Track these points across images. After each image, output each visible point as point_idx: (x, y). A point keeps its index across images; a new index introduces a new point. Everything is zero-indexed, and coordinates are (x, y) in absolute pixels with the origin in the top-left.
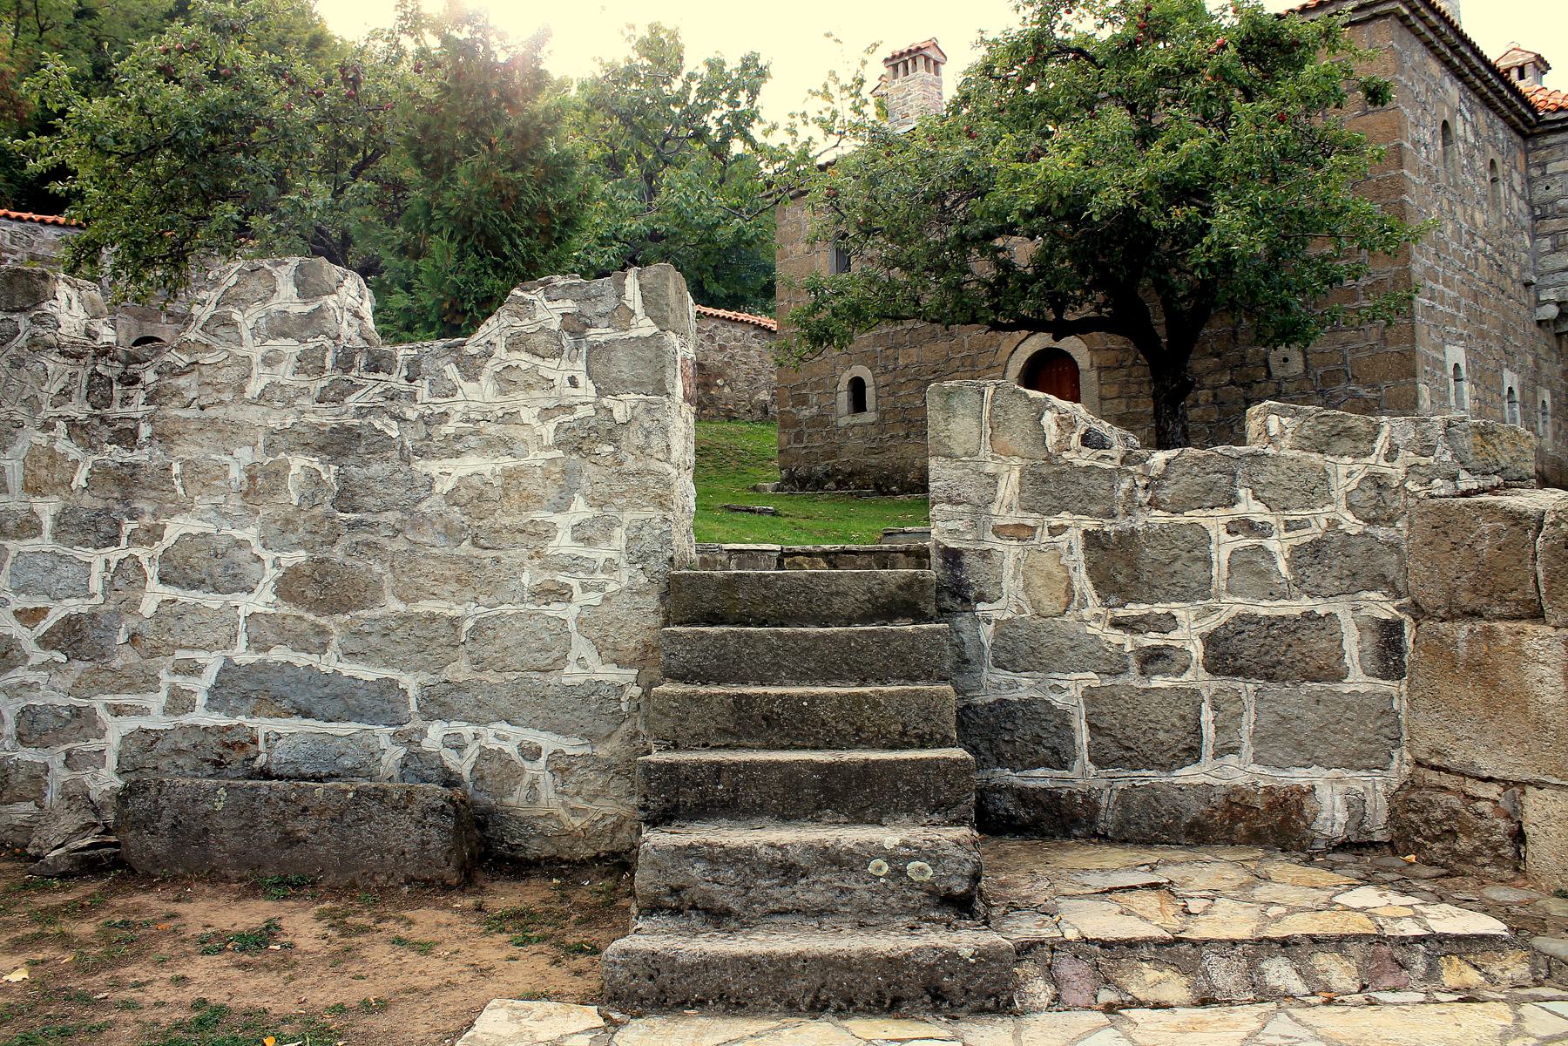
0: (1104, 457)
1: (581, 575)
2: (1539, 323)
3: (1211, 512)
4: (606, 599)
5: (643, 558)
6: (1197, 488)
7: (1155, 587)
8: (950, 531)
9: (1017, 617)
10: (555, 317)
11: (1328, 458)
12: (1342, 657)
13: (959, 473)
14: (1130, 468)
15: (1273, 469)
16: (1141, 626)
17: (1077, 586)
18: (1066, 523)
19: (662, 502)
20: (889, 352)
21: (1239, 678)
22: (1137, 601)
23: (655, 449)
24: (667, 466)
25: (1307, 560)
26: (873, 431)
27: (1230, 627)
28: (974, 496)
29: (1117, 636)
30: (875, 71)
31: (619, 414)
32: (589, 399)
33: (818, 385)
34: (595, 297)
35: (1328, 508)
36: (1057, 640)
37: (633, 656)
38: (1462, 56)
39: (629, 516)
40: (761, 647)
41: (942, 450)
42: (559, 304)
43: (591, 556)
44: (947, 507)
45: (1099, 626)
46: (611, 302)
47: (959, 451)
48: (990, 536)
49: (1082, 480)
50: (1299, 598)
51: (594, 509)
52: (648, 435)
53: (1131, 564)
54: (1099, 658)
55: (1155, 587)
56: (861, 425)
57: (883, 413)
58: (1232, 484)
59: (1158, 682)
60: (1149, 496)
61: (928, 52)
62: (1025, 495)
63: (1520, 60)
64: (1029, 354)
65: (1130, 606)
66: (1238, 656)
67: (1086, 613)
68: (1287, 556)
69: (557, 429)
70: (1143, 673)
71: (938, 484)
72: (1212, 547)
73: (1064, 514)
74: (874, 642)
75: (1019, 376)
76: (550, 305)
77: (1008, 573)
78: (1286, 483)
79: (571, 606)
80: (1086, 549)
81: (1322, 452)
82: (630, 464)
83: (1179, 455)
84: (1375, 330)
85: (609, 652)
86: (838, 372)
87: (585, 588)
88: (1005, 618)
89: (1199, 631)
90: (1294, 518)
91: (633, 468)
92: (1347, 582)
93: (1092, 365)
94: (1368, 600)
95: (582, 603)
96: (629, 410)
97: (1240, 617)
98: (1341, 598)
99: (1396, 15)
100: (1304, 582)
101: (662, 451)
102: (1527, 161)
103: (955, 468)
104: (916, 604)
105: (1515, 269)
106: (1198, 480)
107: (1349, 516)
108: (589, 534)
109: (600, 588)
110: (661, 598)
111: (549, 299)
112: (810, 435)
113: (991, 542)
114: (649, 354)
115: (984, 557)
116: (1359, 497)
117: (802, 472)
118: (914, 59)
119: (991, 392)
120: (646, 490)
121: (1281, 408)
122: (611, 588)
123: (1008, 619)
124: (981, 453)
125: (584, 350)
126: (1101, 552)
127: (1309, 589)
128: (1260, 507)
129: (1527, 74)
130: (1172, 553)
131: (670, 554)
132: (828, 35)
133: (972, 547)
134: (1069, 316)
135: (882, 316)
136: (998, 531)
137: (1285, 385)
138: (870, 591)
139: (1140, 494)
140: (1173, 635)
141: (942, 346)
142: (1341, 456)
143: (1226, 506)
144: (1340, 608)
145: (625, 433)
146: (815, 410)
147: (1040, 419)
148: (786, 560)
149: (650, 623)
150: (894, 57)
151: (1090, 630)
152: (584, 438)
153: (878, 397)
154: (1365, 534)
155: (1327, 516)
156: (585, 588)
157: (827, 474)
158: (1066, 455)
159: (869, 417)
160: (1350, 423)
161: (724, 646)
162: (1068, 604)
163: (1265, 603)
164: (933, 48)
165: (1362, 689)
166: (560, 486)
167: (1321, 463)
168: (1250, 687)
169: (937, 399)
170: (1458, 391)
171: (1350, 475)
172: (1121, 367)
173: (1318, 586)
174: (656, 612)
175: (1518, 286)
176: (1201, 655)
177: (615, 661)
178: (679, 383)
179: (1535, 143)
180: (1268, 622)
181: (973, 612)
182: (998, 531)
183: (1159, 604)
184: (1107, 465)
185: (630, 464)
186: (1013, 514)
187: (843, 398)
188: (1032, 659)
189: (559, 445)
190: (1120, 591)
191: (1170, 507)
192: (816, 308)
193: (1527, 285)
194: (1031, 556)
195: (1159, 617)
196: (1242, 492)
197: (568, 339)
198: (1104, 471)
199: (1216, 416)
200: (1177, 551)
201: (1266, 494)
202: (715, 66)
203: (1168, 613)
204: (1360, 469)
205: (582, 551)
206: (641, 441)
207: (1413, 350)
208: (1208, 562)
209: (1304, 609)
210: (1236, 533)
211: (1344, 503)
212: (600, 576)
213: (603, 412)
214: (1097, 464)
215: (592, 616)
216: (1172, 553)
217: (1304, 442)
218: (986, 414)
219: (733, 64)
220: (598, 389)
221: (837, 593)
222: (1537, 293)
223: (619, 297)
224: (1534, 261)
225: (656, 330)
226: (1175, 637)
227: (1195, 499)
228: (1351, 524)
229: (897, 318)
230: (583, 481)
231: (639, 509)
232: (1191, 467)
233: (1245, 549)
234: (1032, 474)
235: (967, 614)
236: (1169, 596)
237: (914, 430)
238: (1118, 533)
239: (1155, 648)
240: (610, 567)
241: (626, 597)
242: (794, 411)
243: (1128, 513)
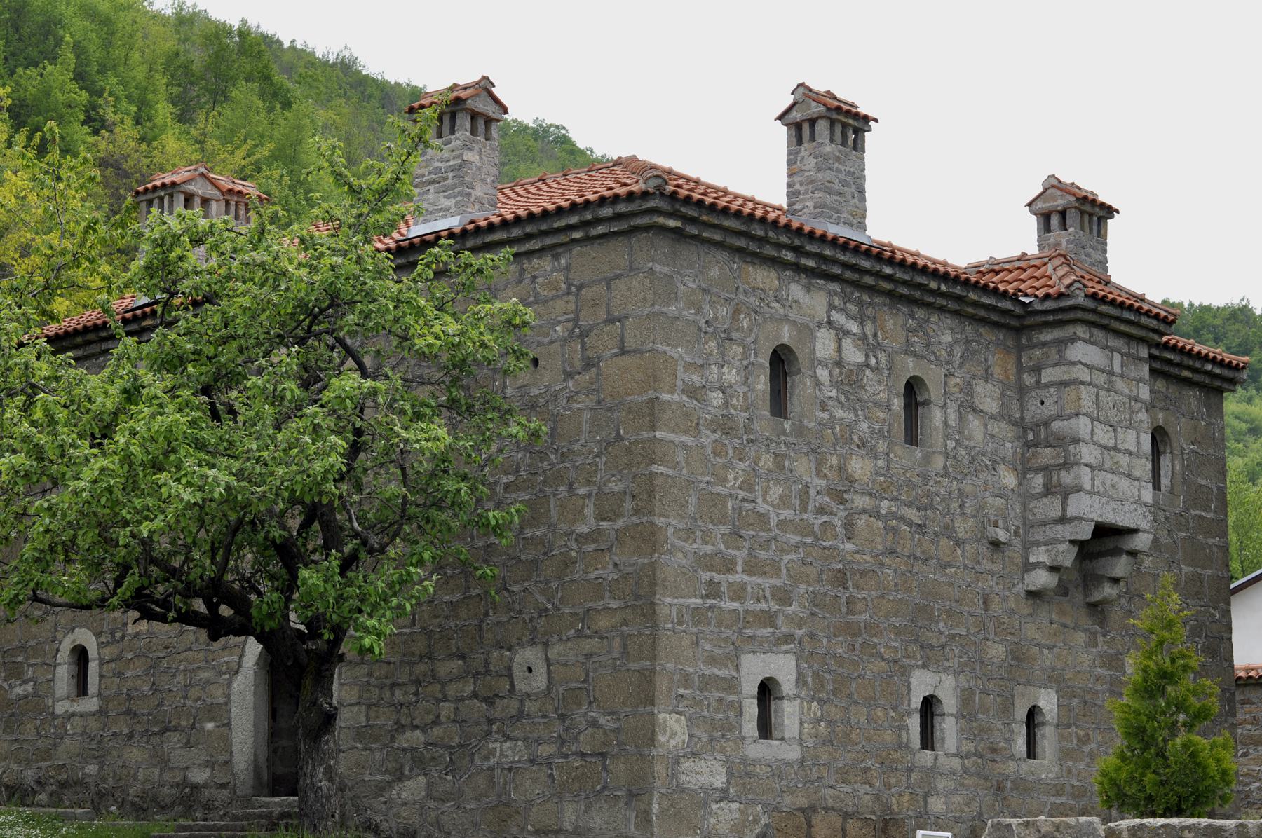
61: (190, 188)
63: (1060, 203)
86: (59, 635)
105: (963, 528)
118: (171, 196)
129: (1069, 222)
137: (528, 703)
146: (29, 687)
153: (101, 676)
164: (200, 181)
179: (1029, 339)
187: (64, 673)
199: (457, 740)
224: (1024, 506)
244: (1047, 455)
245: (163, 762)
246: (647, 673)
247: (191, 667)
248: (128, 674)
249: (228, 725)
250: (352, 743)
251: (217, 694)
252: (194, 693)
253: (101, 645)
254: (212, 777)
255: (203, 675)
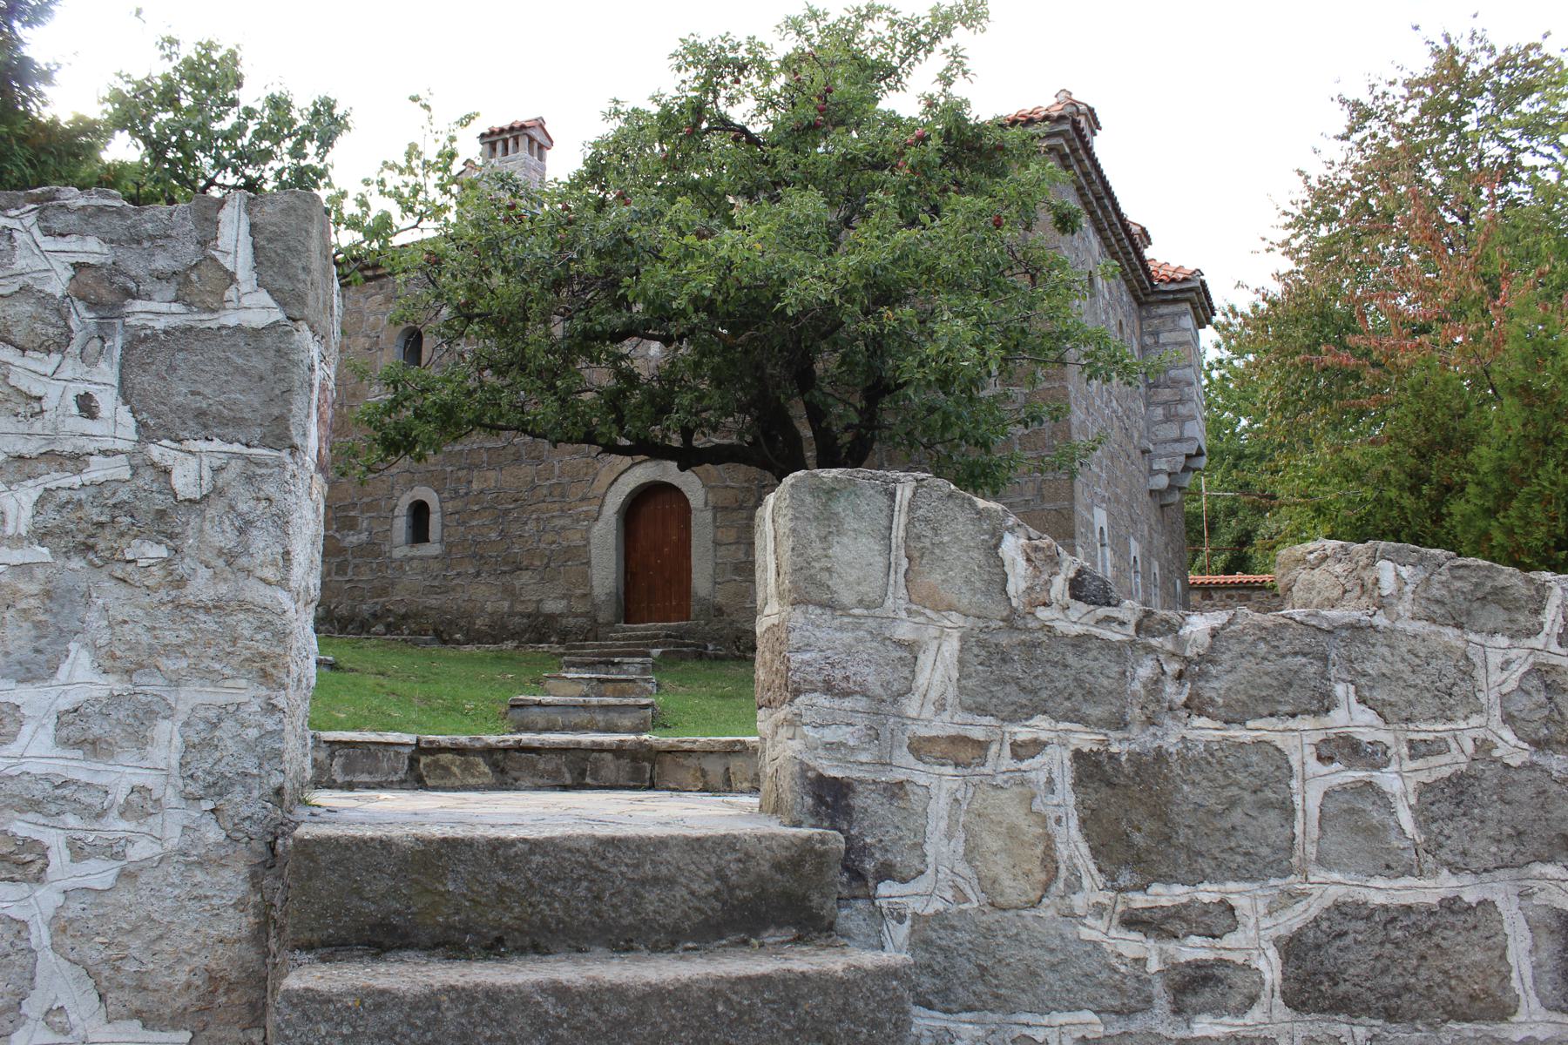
0: (1108, 619)
1: (71, 820)
2: (1151, 492)
3: (1291, 723)
4: (126, 875)
5: (218, 787)
6: (1266, 679)
7: (1200, 854)
8: (830, 746)
9: (953, 909)
10: (59, 268)
11: (1472, 636)
12: (1506, 978)
13: (847, 637)
14: (1154, 642)
15: (1386, 651)
16: (1176, 926)
17: (1062, 852)
18: (1043, 736)
19: (267, 671)
20: (461, 474)
21: (1342, 1017)
22: (1168, 879)
23: (259, 558)
24: (283, 596)
25: (1446, 808)
26: (435, 566)
27: (1325, 925)
28: (873, 682)
29: (1132, 944)
30: (470, 148)
31: (186, 479)
32: (120, 445)
33: (369, 507)
34: (152, 238)
35: (1475, 720)
36: (1027, 952)
37: (180, 1002)
38: (1104, 208)
39: (194, 696)
40: (520, 1022)
41: (815, 594)
42: (71, 243)
43: (97, 780)
44: (823, 701)
45: (1101, 924)
46: (189, 252)
47: (847, 597)
48: (903, 757)
49: (1071, 659)
50: (1435, 873)
51: (112, 678)
52: (245, 527)
53: (1160, 813)
54: (1102, 985)
55: (1200, 854)
56: (422, 558)
57: (450, 546)
58: (1324, 676)
59: (1205, 1026)
60: (1187, 691)
61: (533, 133)
62: (970, 683)
64: (632, 486)
65: (1156, 888)
66: (1339, 978)
67: (1079, 902)
68: (1413, 801)
69: (40, 503)
70: (1178, 1011)
71: (807, 656)
72: (1295, 784)
73: (1041, 721)
74: (765, 1002)
75: (618, 512)
76: (48, 244)
77: (937, 826)
78: (1412, 679)
79: (41, 891)
80: (1079, 783)
81: (1459, 626)
82: (202, 587)
83: (1230, 622)
84: (1031, 484)
85: (125, 995)
86: (397, 494)
87: (78, 851)
88: (930, 910)
89: (1274, 933)
90: (1423, 736)
91: (207, 595)
92: (1510, 847)
93: (706, 504)
94: (1543, 877)
95: (68, 884)
96: (207, 474)
97: (1338, 907)
98: (1501, 874)
99: (1058, 151)
100: (1440, 846)
101: (274, 563)
102: (1141, 328)
103: (841, 629)
104: (806, 898)
106: (1267, 664)
107: (1507, 734)
108: (96, 731)
109: (113, 851)
110: (254, 875)
111: (48, 232)
112: (356, 566)
113: (906, 767)
114: (259, 364)
115: (893, 796)
116: (1521, 704)
117: (343, 610)
118: (516, 139)
119: (908, 493)
120: (234, 641)
121: (1398, 551)
122: (141, 850)
123: (937, 913)
124: (889, 603)
125: (117, 343)
126: (1105, 792)
127: (1450, 858)
128: (1369, 716)
130: (1227, 793)
131: (276, 780)
132: (414, 99)
133: (869, 777)
134: (699, 441)
135: (477, 423)
136: (919, 748)
138: (720, 875)
139: (1170, 688)
140: (1230, 940)
141: (527, 471)
142: (1493, 633)
143: (1316, 714)
144: (1500, 891)
145: (194, 521)
146: (364, 536)
147: (997, 546)
148: (424, 760)
149: (226, 928)
150: (492, 133)
151: (1086, 934)
152: (101, 525)
153: (444, 526)
154: (1532, 766)
155: (1474, 733)
156: (78, 851)
157: (374, 615)
158: (1043, 613)
159: (432, 549)
160: (1501, 581)
161: (431, 1023)
162: (1046, 887)
163: (1379, 882)
164: (539, 130)
165: (1541, 1033)
166: (37, 625)
167: (1460, 644)
168: (1360, 1032)
169: (808, 499)
170: (1103, 554)
171: (1504, 666)
172: (741, 508)
173: (1464, 853)
174: (240, 905)
175: (1138, 452)
176: (1278, 976)
177: (138, 1014)
178: (314, 431)
179: (1149, 312)
180: (1385, 917)
181: (871, 898)
182: (919, 748)
183: (1206, 886)
184: (1114, 635)
185: (202, 587)
186: (946, 716)
187: (401, 525)
188: (980, 988)
189: (42, 535)
190: (1139, 860)
191: (1222, 712)
192: (395, 405)
193: (1145, 452)
194: (979, 795)
195: (1206, 909)
196: (1340, 690)
197: (82, 319)
198: (1107, 645)
200: (1235, 791)
201: (1378, 694)
202: (279, 105)
203: (1222, 902)
204: (1522, 656)
205: (77, 767)
206: (228, 539)
207: (1072, 509)
208: (1287, 810)
209: (1444, 893)
210: (1331, 759)
211: (1498, 712)
212: (118, 826)
213: (147, 475)
214: (1096, 631)
215: (89, 914)
216: (1227, 793)
217: (1435, 607)
218: (899, 533)
219: (300, 115)
220: (142, 426)
221: (656, 880)
222: (1151, 460)
223: (203, 244)
225: (278, 315)
226: (1234, 946)
227: (1264, 699)
228: (1511, 748)
229: (493, 428)
230: (92, 616)
231: (214, 683)
232: (1254, 644)
233: (1344, 789)
234: (982, 645)
235: (860, 904)
236: (1223, 871)
237: (486, 567)
238: (1135, 758)
239: (1199, 965)
240: (141, 804)
241: (173, 872)
242: (338, 535)
243: (1150, 721)
244: (1166, 394)
245: (510, 592)
246: (1065, 512)
247: (544, 516)
248: (474, 523)
249: (588, 563)
250: (729, 576)
251: (575, 538)
252: (549, 537)
253: (441, 501)
254: (569, 607)
255: (561, 522)
